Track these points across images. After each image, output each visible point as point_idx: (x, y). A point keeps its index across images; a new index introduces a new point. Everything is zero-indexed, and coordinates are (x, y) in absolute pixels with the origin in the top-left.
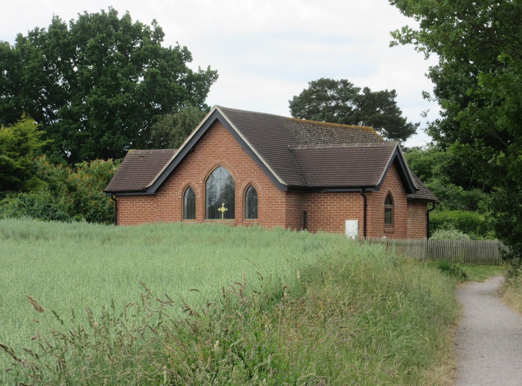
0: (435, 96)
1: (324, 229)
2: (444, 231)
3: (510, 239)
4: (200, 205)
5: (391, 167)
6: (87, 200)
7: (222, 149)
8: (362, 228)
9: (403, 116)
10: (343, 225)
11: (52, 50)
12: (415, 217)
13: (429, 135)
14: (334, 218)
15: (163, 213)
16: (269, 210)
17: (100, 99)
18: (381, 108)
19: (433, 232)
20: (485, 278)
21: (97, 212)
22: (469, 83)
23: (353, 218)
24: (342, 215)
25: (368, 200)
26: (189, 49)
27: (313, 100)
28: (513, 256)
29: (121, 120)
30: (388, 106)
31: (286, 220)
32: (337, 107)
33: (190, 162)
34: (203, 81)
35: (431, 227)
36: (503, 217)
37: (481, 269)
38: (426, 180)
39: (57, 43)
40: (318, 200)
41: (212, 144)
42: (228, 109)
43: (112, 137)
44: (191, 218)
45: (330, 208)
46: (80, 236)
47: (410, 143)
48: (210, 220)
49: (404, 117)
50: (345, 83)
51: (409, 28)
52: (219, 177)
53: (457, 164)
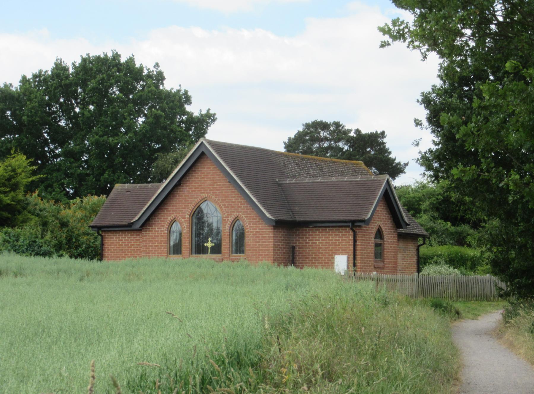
0: (428, 124)
1: (312, 264)
2: (434, 266)
3: (507, 275)
4: (186, 240)
5: (381, 201)
6: (79, 235)
7: (209, 183)
9: (392, 156)
11: (54, 90)
13: (422, 165)
14: (322, 253)
16: (256, 245)
17: (101, 139)
18: (372, 148)
19: (423, 267)
20: (479, 315)
21: (89, 247)
22: (464, 109)
25: (358, 235)
27: (307, 140)
28: (510, 293)
29: (121, 159)
30: (377, 146)
31: (274, 255)
32: (330, 147)
33: (176, 196)
34: (202, 123)
35: (422, 262)
36: (500, 252)
37: (472, 305)
39: (58, 84)
40: (312, 235)
42: (215, 142)
43: (112, 175)
44: (178, 254)
46: (58, 273)
47: (398, 182)
48: (197, 255)
49: (394, 158)
50: (337, 124)
51: (401, 20)
53: (446, 200)
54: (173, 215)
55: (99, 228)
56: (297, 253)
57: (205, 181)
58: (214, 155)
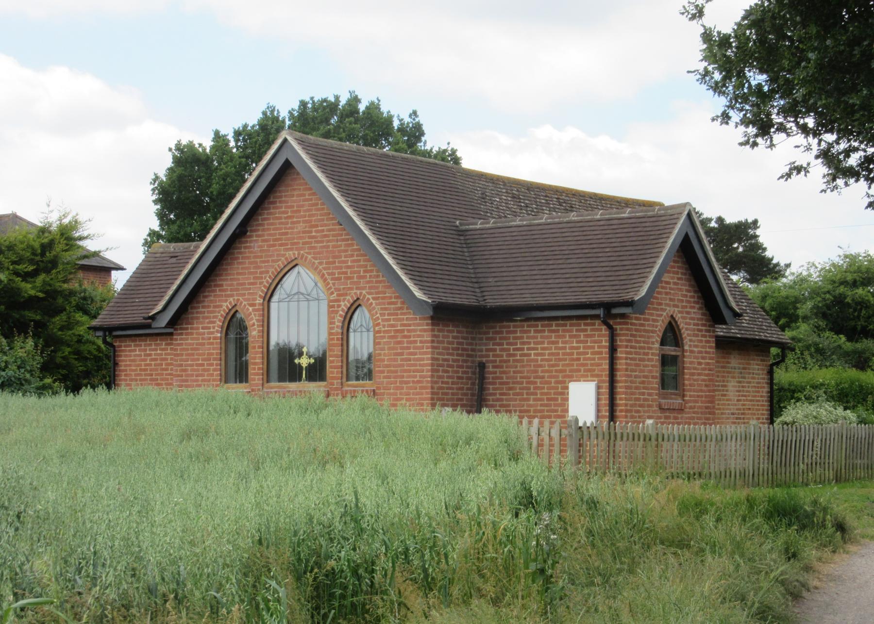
4: (257, 353)
7: (300, 227)
8: (605, 401)
10: (564, 395)
12: (744, 378)
14: (543, 377)
15: (185, 370)
18: (740, 243)
23: (587, 376)
24: (561, 371)
25: (619, 335)
26: (459, 154)
30: (747, 240)
33: (238, 258)
35: (778, 399)
38: (789, 327)
41: (280, 218)
44: (241, 382)
45: (536, 355)
49: (770, 256)
52: (295, 291)
54: (231, 299)
55: (108, 330)
56: (490, 377)
57: (293, 223)
58: (309, 168)
